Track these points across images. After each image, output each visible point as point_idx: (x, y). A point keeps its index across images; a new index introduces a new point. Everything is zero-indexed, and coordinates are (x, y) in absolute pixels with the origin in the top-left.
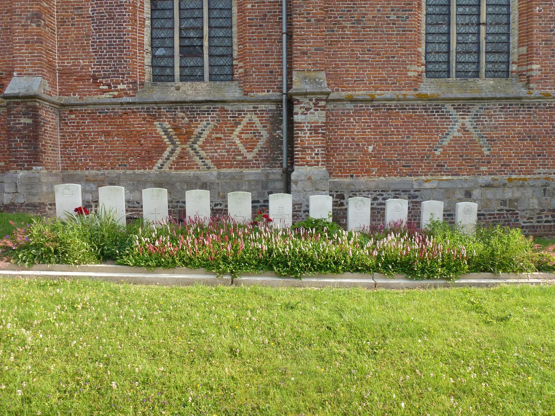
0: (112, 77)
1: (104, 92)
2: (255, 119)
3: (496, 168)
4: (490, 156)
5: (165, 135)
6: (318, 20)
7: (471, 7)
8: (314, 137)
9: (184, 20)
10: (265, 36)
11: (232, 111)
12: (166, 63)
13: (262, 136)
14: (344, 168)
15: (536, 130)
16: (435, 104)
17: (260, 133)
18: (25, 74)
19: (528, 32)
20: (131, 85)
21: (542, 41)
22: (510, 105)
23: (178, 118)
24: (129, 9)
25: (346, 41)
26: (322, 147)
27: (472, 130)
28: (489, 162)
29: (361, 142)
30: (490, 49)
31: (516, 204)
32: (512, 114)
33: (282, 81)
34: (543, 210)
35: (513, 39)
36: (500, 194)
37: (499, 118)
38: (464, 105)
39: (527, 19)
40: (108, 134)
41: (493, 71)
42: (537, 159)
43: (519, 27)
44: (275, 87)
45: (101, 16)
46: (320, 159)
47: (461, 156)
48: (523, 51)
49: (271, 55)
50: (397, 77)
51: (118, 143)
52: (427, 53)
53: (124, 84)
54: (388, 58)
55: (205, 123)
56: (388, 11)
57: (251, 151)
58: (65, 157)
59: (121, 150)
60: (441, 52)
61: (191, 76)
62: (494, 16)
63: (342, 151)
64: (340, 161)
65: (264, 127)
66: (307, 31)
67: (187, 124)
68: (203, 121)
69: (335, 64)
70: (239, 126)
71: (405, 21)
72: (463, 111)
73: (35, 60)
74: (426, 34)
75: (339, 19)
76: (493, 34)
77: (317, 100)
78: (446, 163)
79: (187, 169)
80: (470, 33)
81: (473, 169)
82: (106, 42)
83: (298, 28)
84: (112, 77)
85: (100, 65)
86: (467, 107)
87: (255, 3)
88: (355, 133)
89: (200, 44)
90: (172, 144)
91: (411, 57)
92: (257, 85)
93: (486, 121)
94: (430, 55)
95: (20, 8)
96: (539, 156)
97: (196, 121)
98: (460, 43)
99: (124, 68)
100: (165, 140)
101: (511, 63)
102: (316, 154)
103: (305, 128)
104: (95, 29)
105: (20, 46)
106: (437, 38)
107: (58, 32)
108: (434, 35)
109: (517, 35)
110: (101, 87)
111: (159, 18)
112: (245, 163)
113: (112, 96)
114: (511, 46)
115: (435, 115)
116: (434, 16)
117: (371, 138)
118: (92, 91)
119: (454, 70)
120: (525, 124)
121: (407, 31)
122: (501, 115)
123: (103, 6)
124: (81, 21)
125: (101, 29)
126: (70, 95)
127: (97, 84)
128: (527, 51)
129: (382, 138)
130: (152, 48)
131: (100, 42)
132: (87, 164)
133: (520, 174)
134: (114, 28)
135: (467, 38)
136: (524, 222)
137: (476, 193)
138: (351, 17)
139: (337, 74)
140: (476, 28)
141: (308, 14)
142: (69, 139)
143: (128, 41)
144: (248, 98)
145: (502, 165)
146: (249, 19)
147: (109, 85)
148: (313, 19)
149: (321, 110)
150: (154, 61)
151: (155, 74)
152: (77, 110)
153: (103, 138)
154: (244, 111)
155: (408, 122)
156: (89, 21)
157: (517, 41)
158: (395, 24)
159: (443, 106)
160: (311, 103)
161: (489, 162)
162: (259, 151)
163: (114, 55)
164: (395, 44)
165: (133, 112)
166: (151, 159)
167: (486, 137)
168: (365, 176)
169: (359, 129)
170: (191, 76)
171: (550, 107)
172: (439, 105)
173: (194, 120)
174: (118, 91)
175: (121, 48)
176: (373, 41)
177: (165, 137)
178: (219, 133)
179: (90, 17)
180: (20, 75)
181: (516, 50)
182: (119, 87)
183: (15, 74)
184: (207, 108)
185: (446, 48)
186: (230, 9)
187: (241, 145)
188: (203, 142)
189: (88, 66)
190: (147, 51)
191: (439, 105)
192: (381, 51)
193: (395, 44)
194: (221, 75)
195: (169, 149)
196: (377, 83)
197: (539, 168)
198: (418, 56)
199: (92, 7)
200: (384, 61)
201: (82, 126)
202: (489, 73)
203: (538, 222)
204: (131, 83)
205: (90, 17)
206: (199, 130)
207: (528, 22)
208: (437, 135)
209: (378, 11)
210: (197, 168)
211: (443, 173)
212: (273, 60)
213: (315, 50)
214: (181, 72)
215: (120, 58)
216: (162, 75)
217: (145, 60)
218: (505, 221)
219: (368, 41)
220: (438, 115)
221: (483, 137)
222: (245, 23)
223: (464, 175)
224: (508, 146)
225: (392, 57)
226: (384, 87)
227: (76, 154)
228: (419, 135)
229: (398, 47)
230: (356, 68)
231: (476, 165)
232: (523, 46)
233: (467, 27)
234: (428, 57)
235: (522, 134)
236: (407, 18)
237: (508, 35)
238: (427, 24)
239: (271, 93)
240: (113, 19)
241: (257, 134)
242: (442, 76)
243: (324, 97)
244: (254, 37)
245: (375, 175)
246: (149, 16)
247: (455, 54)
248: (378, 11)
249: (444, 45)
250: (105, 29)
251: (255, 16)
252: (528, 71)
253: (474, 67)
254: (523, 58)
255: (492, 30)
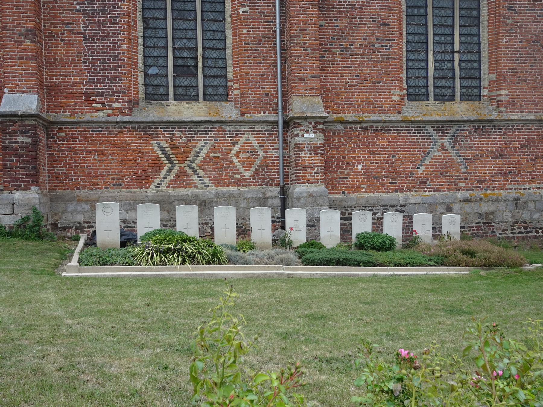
0: (106, 95)
1: (97, 110)
2: (252, 139)
3: (473, 184)
4: (467, 173)
5: (163, 154)
6: (314, 50)
7: (446, 36)
8: (314, 157)
9: (178, 40)
10: (260, 60)
11: (230, 131)
12: (160, 82)
13: (259, 155)
14: (336, 185)
15: (507, 150)
16: (417, 127)
17: (257, 152)
18: (18, 91)
19: (496, 61)
20: (126, 104)
21: (509, 69)
22: (483, 127)
23: (176, 137)
24: (124, 28)
25: (336, 67)
26: (321, 166)
27: (450, 149)
28: (466, 179)
29: (352, 161)
30: (464, 75)
31: (492, 217)
32: (485, 135)
33: (278, 103)
34: (516, 223)
35: (484, 66)
36: (476, 208)
37: (474, 138)
38: (442, 127)
39: (496, 49)
40: (102, 153)
41: (467, 95)
42: (508, 175)
43: (489, 56)
44: (271, 108)
45: (94, 33)
46: (320, 177)
47: (441, 174)
48: (493, 78)
49: (266, 78)
50: (382, 101)
51: (112, 161)
52: (408, 78)
53: (120, 102)
54: (374, 83)
55: (203, 142)
56: (374, 40)
57: (249, 170)
58: (52, 177)
59: (116, 169)
60: (420, 77)
61: (185, 95)
62: (466, 45)
63: (334, 169)
64: (332, 179)
65: (260, 146)
66: (304, 60)
67: (185, 143)
68: (201, 140)
69: (326, 88)
70: (236, 146)
71: (389, 49)
72: (442, 133)
73: (30, 77)
74: (407, 60)
75: (329, 46)
76: (466, 61)
77: (316, 123)
78: (428, 180)
79: (185, 187)
80: (446, 60)
81: (452, 185)
82: (99, 59)
83: (295, 56)
84: (106, 95)
85: (94, 83)
86: (445, 128)
87: (250, 28)
88: (346, 152)
89: (193, 64)
90: (170, 163)
91: (395, 83)
92: (254, 107)
93: (462, 141)
94: (411, 80)
95: (11, 23)
96: (510, 173)
97: (194, 140)
98: (438, 69)
99: (119, 86)
100: (163, 159)
101: (482, 87)
102: (315, 173)
103: (305, 149)
104: (87, 46)
105: (11, 62)
106: (417, 64)
107: (45, 47)
108: (414, 62)
109: (487, 63)
110: (93, 105)
111: (151, 37)
112: (242, 182)
113: (106, 115)
114: (482, 72)
115: (417, 136)
116: (413, 44)
117: (360, 157)
118: (84, 109)
119: (432, 94)
120: (497, 144)
121: (390, 58)
122: (475, 135)
123: (96, 23)
124: (72, 37)
125: (94, 46)
126: (60, 112)
127: (89, 102)
128: (497, 78)
129: (370, 157)
130: (145, 66)
131: (92, 59)
132: (78, 183)
133: (494, 190)
134: (108, 46)
135: (443, 64)
136: (500, 234)
137: (456, 207)
138: (340, 45)
139: (329, 98)
140: (451, 56)
141: (305, 43)
142: (58, 157)
143: (124, 60)
144: (245, 118)
145: (478, 182)
146: (245, 44)
147: (103, 103)
148: (309, 49)
149: (319, 132)
150: (146, 79)
151: (148, 92)
152: (68, 128)
153: (96, 157)
154: (241, 131)
155: (393, 142)
156: (80, 37)
157: (487, 68)
158: (380, 52)
159: (424, 127)
160: (311, 126)
161: (466, 179)
162: (256, 169)
163: (108, 73)
164: (380, 70)
165: (129, 131)
166: (147, 178)
167: (463, 156)
168: (356, 192)
169: (349, 149)
170: (185, 95)
171: (518, 129)
172: (420, 127)
173: (192, 139)
174: (112, 109)
175: (115, 66)
176: (360, 67)
177: (163, 156)
178: (216, 153)
179: (82, 33)
180: (12, 91)
181: (486, 76)
182: (115, 105)
183: (6, 90)
184: (205, 128)
185: (425, 73)
186: (224, 32)
187: (238, 164)
188: (201, 161)
189: (79, 83)
190: (140, 70)
191: (420, 127)
192: (368, 77)
193: (380, 70)
194: (215, 95)
195: (166, 168)
196: (365, 107)
197: (511, 184)
198: (401, 81)
199: (84, 24)
200: (370, 86)
201: (73, 144)
202: (463, 97)
203: (512, 233)
204: (127, 102)
205: (82, 33)
206: (197, 149)
207: (496, 52)
208: (420, 154)
209: (365, 39)
210: (195, 187)
211: (426, 189)
212: (269, 83)
213: (312, 77)
214: (174, 91)
215: (114, 76)
216: (156, 94)
217: (139, 78)
218: (484, 233)
219: (356, 67)
220: (420, 136)
221: (460, 156)
222: (240, 47)
223: (445, 191)
224: (482, 164)
225: (378, 83)
226: (371, 110)
227: (65, 173)
228: (403, 154)
229: (383, 73)
230: (346, 92)
231: (455, 182)
232: (494, 73)
233: (443, 54)
234: (409, 81)
235: (495, 153)
236: (391, 46)
237: (479, 61)
238: (407, 51)
239: (267, 114)
240: (107, 36)
241: (253, 153)
242: (422, 98)
243: (322, 121)
244: (250, 61)
245: (364, 192)
246: (142, 34)
247: (433, 79)
248: (365, 39)
249: (423, 71)
250: (99, 46)
251: (251, 41)
252: (497, 96)
253: (450, 91)
254: (492, 84)
255: (465, 57)
